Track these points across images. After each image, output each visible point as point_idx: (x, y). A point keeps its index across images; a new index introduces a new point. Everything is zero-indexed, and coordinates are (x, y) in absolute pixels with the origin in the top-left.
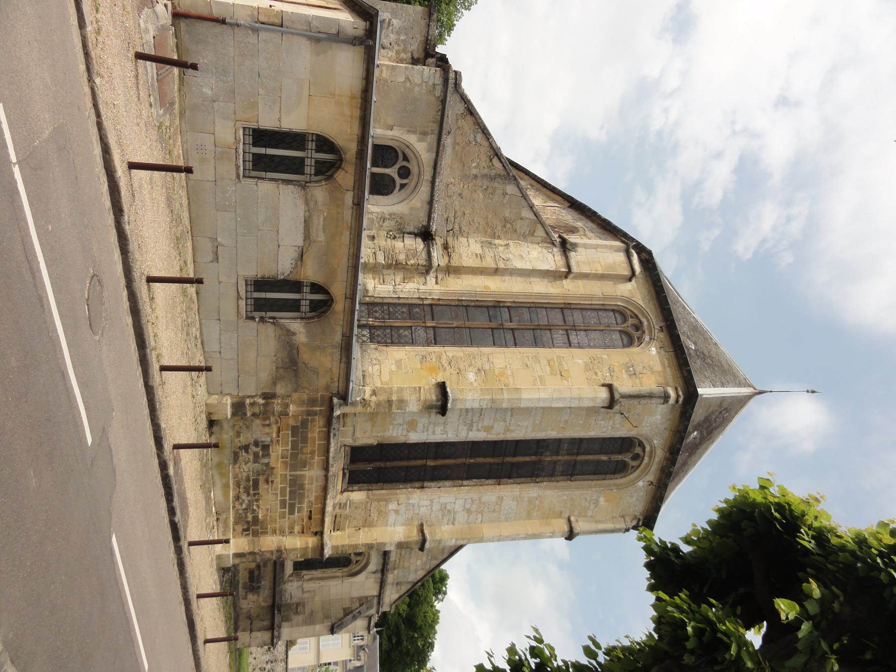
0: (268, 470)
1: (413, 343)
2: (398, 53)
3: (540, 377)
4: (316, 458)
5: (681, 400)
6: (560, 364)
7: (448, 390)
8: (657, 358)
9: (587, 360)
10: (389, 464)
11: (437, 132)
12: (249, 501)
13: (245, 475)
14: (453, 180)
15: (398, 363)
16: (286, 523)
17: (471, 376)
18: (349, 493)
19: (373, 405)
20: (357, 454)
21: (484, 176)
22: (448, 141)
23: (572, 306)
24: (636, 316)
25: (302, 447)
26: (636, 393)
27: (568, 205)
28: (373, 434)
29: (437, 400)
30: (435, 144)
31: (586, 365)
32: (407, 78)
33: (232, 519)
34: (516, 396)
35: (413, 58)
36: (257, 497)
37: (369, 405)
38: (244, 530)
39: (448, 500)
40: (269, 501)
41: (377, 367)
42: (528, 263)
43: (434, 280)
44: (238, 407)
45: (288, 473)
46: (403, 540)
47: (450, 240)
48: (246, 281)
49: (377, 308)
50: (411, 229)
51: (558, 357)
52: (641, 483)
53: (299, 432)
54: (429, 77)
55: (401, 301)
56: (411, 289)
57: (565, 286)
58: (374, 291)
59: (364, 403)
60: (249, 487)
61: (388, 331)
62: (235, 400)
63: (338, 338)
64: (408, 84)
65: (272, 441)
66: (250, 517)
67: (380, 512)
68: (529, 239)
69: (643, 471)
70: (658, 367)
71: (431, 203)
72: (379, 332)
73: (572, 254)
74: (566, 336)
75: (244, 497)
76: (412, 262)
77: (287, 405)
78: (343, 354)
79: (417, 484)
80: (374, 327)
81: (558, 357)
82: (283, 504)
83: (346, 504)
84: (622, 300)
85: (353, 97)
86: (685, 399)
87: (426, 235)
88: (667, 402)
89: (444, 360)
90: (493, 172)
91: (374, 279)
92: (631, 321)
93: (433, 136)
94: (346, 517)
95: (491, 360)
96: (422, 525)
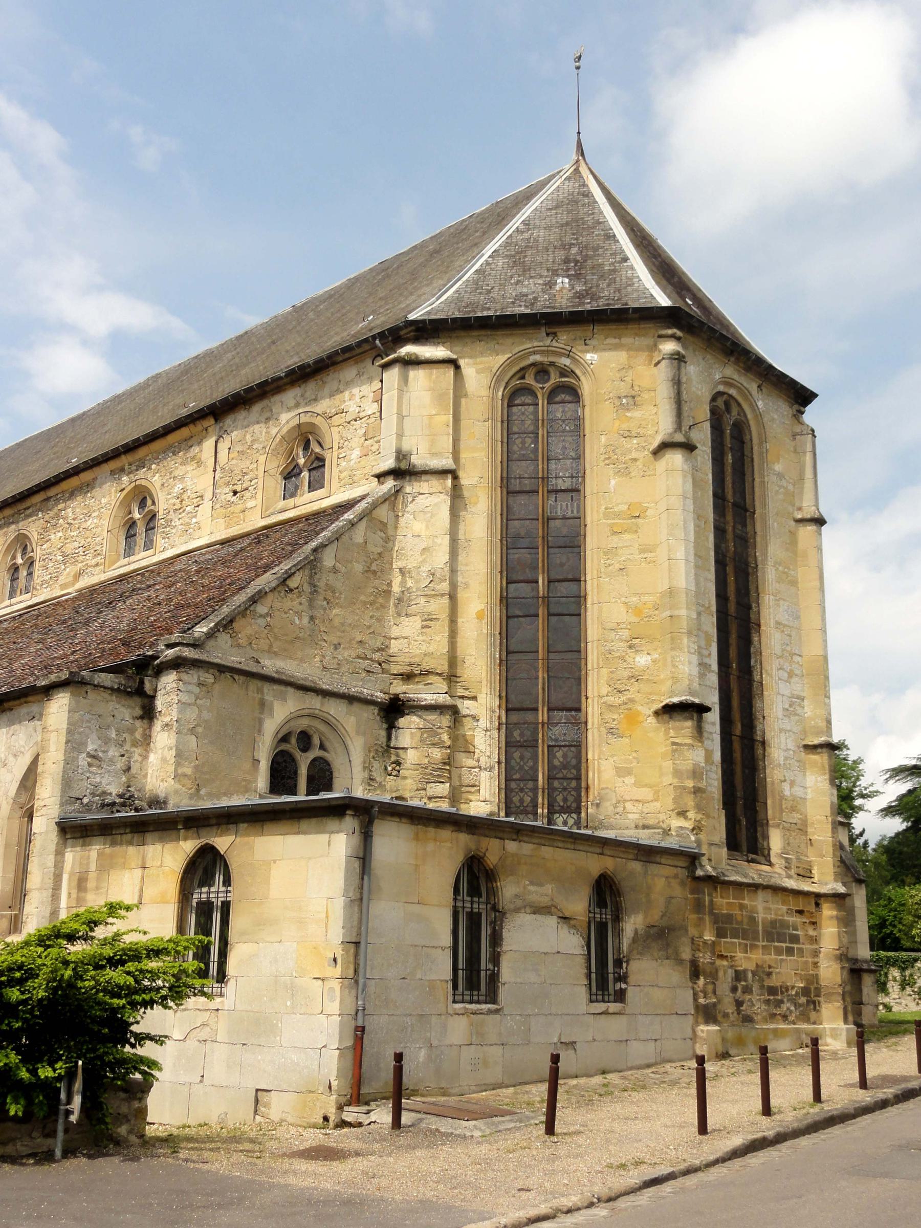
1: (578, 747)
2: (135, 744)
4: (746, 902)
5: (679, 333)
6: (618, 515)
7: (676, 700)
8: (606, 354)
9: (610, 470)
10: (739, 794)
11: (259, 683)
12: (788, 1000)
13: (764, 1007)
14: (318, 659)
15: (622, 772)
16: (807, 947)
17: (642, 660)
18: (772, 853)
19: (699, 816)
20: (733, 844)
21: (311, 601)
22: (269, 665)
23: (505, 475)
24: (522, 369)
25: (737, 923)
26: (674, 406)
27: (212, 421)
28: (716, 816)
29: (692, 719)
30: (276, 687)
31: (618, 473)
32: (192, 731)
33: (805, 1026)
34: (683, 598)
35: (142, 718)
37: (699, 821)
38: (815, 1009)
39: (780, 706)
40: (788, 972)
41: (629, 805)
42: (439, 541)
43: (467, 703)
44: (708, 1014)
45: (761, 944)
46: (827, 776)
47: (395, 669)
48: (591, 1001)
49: (516, 799)
50: (383, 733)
51: (606, 516)
53: (724, 926)
54: (189, 692)
55: (503, 759)
56: (485, 741)
57: (474, 481)
58: (491, 802)
59: (697, 829)
60: (776, 1000)
61: (556, 784)
62: (700, 1019)
63: (636, 866)
64: (200, 730)
65: (731, 967)
66: (803, 1000)
67: (793, 809)
68: (390, 532)
69: (746, 399)
70: (622, 356)
72: (559, 799)
73: (418, 460)
74: (559, 495)
75: (784, 1007)
76: (445, 737)
77: (705, 942)
78: (658, 859)
79: (760, 751)
80: (550, 806)
81: (606, 516)
82: (790, 951)
83: (786, 859)
84: (496, 389)
85: (417, 838)
86: (680, 328)
87: (394, 710)
88: (684, 357)
89: (617, 700)
90: (307, 588)
91: (469, 801)
92: (530, 380)
93: (266, 691)
94: (798, 859)
95: (613, 626)
96: (806, 747)
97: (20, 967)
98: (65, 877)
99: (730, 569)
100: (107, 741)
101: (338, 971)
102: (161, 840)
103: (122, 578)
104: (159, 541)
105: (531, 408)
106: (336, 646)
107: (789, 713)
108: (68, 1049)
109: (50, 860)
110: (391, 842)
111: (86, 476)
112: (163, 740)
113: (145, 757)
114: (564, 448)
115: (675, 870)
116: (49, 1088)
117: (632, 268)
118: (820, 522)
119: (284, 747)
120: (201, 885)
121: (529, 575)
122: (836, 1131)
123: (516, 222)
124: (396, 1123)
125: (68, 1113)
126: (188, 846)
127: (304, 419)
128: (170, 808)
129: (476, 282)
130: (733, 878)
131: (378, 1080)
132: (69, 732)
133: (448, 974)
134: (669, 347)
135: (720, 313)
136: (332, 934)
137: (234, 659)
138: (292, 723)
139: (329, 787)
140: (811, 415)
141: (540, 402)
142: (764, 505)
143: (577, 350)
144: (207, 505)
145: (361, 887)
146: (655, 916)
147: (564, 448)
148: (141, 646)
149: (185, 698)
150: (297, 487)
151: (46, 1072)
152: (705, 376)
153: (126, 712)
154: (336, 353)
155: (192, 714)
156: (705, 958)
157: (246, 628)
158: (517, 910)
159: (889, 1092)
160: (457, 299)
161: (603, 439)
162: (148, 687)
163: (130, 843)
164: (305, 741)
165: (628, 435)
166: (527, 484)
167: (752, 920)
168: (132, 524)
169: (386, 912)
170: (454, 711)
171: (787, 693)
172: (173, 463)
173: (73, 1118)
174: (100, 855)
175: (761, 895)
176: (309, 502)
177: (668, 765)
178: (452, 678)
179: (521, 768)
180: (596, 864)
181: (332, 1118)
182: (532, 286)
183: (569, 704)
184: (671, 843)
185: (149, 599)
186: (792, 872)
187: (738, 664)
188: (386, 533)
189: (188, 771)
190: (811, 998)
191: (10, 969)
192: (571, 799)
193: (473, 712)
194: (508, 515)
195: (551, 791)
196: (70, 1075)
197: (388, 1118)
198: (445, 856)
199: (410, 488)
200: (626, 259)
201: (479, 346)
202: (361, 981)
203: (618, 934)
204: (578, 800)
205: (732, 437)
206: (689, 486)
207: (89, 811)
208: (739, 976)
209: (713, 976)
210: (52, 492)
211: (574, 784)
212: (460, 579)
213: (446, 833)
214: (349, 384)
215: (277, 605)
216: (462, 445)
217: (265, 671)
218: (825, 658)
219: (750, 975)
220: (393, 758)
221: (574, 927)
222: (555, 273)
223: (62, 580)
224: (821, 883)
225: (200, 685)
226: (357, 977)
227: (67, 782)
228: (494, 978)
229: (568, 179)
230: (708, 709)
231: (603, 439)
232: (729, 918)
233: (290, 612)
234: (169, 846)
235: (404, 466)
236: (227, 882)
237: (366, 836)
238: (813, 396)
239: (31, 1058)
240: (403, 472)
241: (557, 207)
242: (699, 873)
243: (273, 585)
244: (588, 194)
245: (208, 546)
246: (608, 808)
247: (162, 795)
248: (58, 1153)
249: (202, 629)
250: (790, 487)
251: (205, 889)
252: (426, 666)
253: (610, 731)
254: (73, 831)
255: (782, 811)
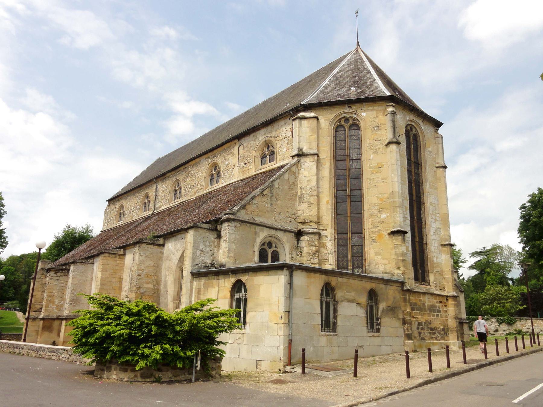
0: (428, 323)
3: (382, 179)
5: (394, 104)
6: (374, 167)
7: (395, 229)
9: (371, 152)
10: (418, 261)
11: (255, 226)
13: (429, 335)
15: (377, 254)
16: (444, 314)
17: (383, 216)
20: (416, 279)
22: (258, 220)
32: (233, 242)
33: (443, 341)
34: (397, 195)
35: (217, 238)
36: (436, 329)
40: (437, 323)
41: (380, 266)
42: (313, 178)
44: (409, 337)
46: (449, 255)
47: (300, 221)
49: (341, 264)
50: (296, 242)
52: (423, 128)
59: (404, 273)
63: (383, 286)
64: (236, 242)
66: (442, 332)
67: (437, 267)
68: (297, 175)
69: (418, 126)
70: (374, 113)
71: (285, 231)
72: (356, 263)
73: (305, 151)
75: (436, 335)
76: (317, 243)
77: (407, 312)
81: (370, 168)
82: (437, 316)
84: (331, 126)
85: (308, 277)
87: (299, 234)
89: (375, 230)
90: (269, 194)
92: (343, 122)
95: (373, 204)
96: (442, 245)
97: (180, 319)
98: (194, 290)
99: (413, 185)
100: (206, 246)
101: (283, 321)
102: (224, 278)
103: (210, 193)
104: (221, 180)
105: (343, 132)
106: (279, 214)
107: (435, 233)
108: (196, 346)
109: (189, 285)
110: (300, 278)
111: (197, 160)
112: (224, 245)
113: (218, 251)
114: (355, 145)
115: (396, 288)
116: (190, 359)
117: (377, 83)
118: (445, 167)
119: (263, 247)
120: (237, 293)
121: (343, 188)
122: (456, 378)
123: (337, 70)
124: (303, 372)
125: (196, 367)
126: (233, 280)
127: (267, 139)
128: (227, 268)
129: (323, 90)
130: (416, 290)
131: (297, 358)
132: (194, 243)
133: (320, 323)
134: (390, 109)
135: (408, 97)
136: (281, 309)
137: (246, 218)
138: (266, 239)
139: (278, 260)
140: (441, 130)
141: (346, 132)
142: (425, 162)
143: (359, 112)
144: (236, 168)
145: (290, 293)
146: (390, 303)
147: (355, 145)
148: (216, 214)
149: (230, 231)
150: (265, 161)
151: (189, 353)
152: (403, 119)
153: (212, 236)
154: (277, 116)
155: (233, 236)
156: (407, 318)
157: (250, 208)
158: (342, 301)
159: (474, 365)
160: (317, 96)
161: (368, 141)
162: (219, 228)
163: (214, 279)
164: (270, 244)
165: (377, 140)
166: (342, 158)
167: (424, 304)
168: (212, 175)
169: (297, 301)
170: (319, 234)
171: (434, 227)
172: (225, 154)
173: (198, 369)
174: (205, 283)
175: (427, 296)
176: (269, 166)
177: (393, 252)
178: (318, 223)
179: (343, 253)
180: (369, 285)
181: (282, 370)
182: (342, 91)
183: (358, 232)
184: (395, 278)
185: (218, 199)
186: (438, 288)
187: (417, 217)
188: (295, 175)
189: (232, 255)
190: (445, 331)
191: (177, 320)
192: (360, 263)
193: (326, 235)
194: (336, 168)
195: (353, 260)
196: (197, 355)
197: (300, 370)
198: (317, 283)
199: (303, 160)
200: (375, 80)
201: (325, 112)
202: (290, 324)
203: (377, 309)
204: (362, 264)
205: (413, 139)
206: (398, 157)
207: (201, 269)
208: (420, 324)
209: (410, 324)
210: (186, 166)
211: (361, 258)
212: (320, 190)
213: (318, 275)
214: (281, 126)
215: (260, 200)
216: (320, 145)
217: (257, 222)
218: (448, 215)
219: (423, 324)
220: (299, 250)
221: (362, 307)
222: (350, 86)
223: (190, 194)
224: (448, 292)
225: (235, 227)
226: (289, 323)
227: (193, 259)
228: (335, 324)
229: (354, 54)
230: (407, 233)
231: (368, 141)
232: (416, 304)
233: (263, 202)
234: (226, 280)
235: (301, 153)
236: (246, 292)
237: (291, 276)
238: (443, 124)
239: (183, 348)
240: (300, 155)
241: (350, 64)
242: (405, 288)
243: (258, 193)
244: (361, 59)
245: (237, 181)
246: (372, 266)
247: (224, 263)
248: (193, 380)
249: (235, 209)
250: (434, 156)
251: (238, 294)
252: (310, 219)
253: (373, 241)
254: (196, 275)
255: (433, 267)
